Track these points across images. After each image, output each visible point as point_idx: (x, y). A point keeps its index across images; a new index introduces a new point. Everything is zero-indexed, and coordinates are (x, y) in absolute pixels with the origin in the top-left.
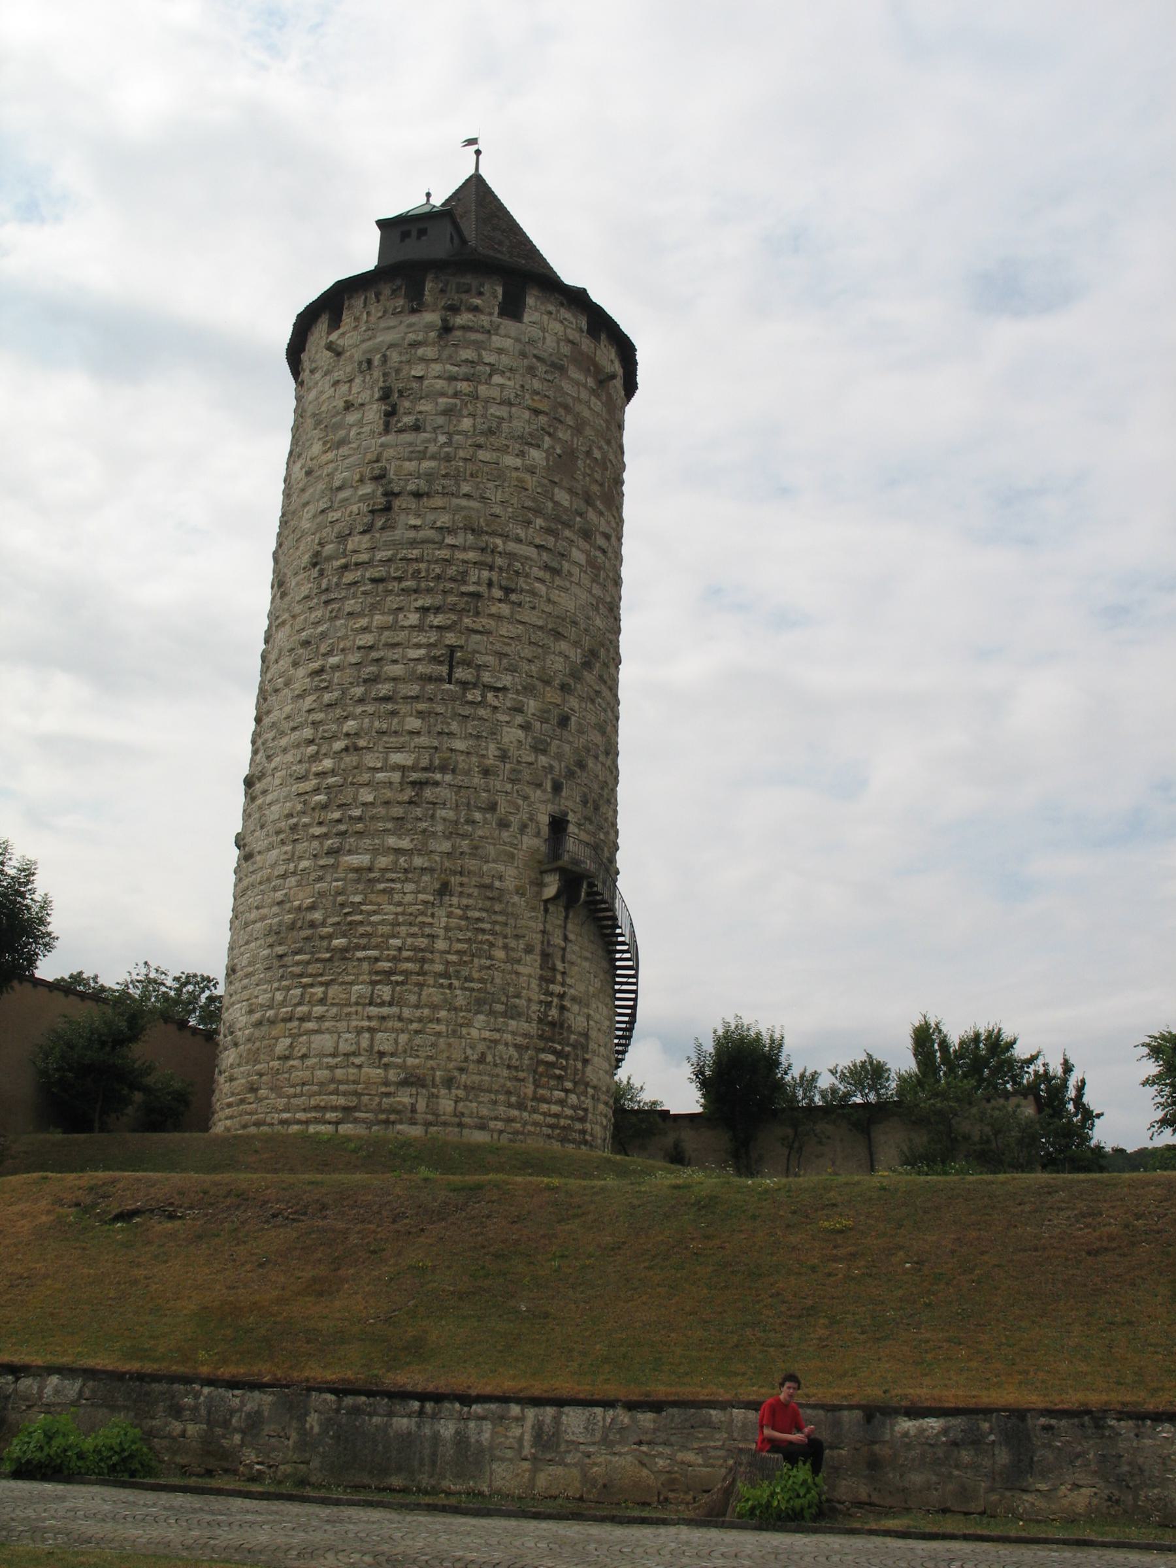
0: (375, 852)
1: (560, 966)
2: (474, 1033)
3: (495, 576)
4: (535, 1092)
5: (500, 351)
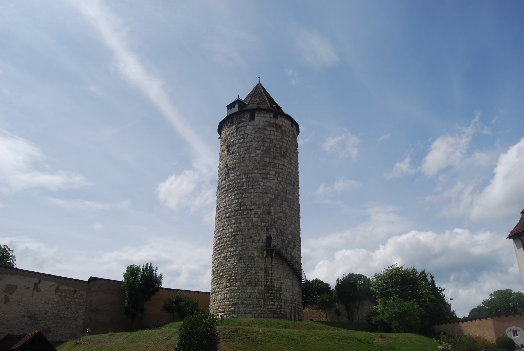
0: (227, 252)
1: (270, 272)
2: (248, 291)
3: (250, 183)
5: (249, 130)
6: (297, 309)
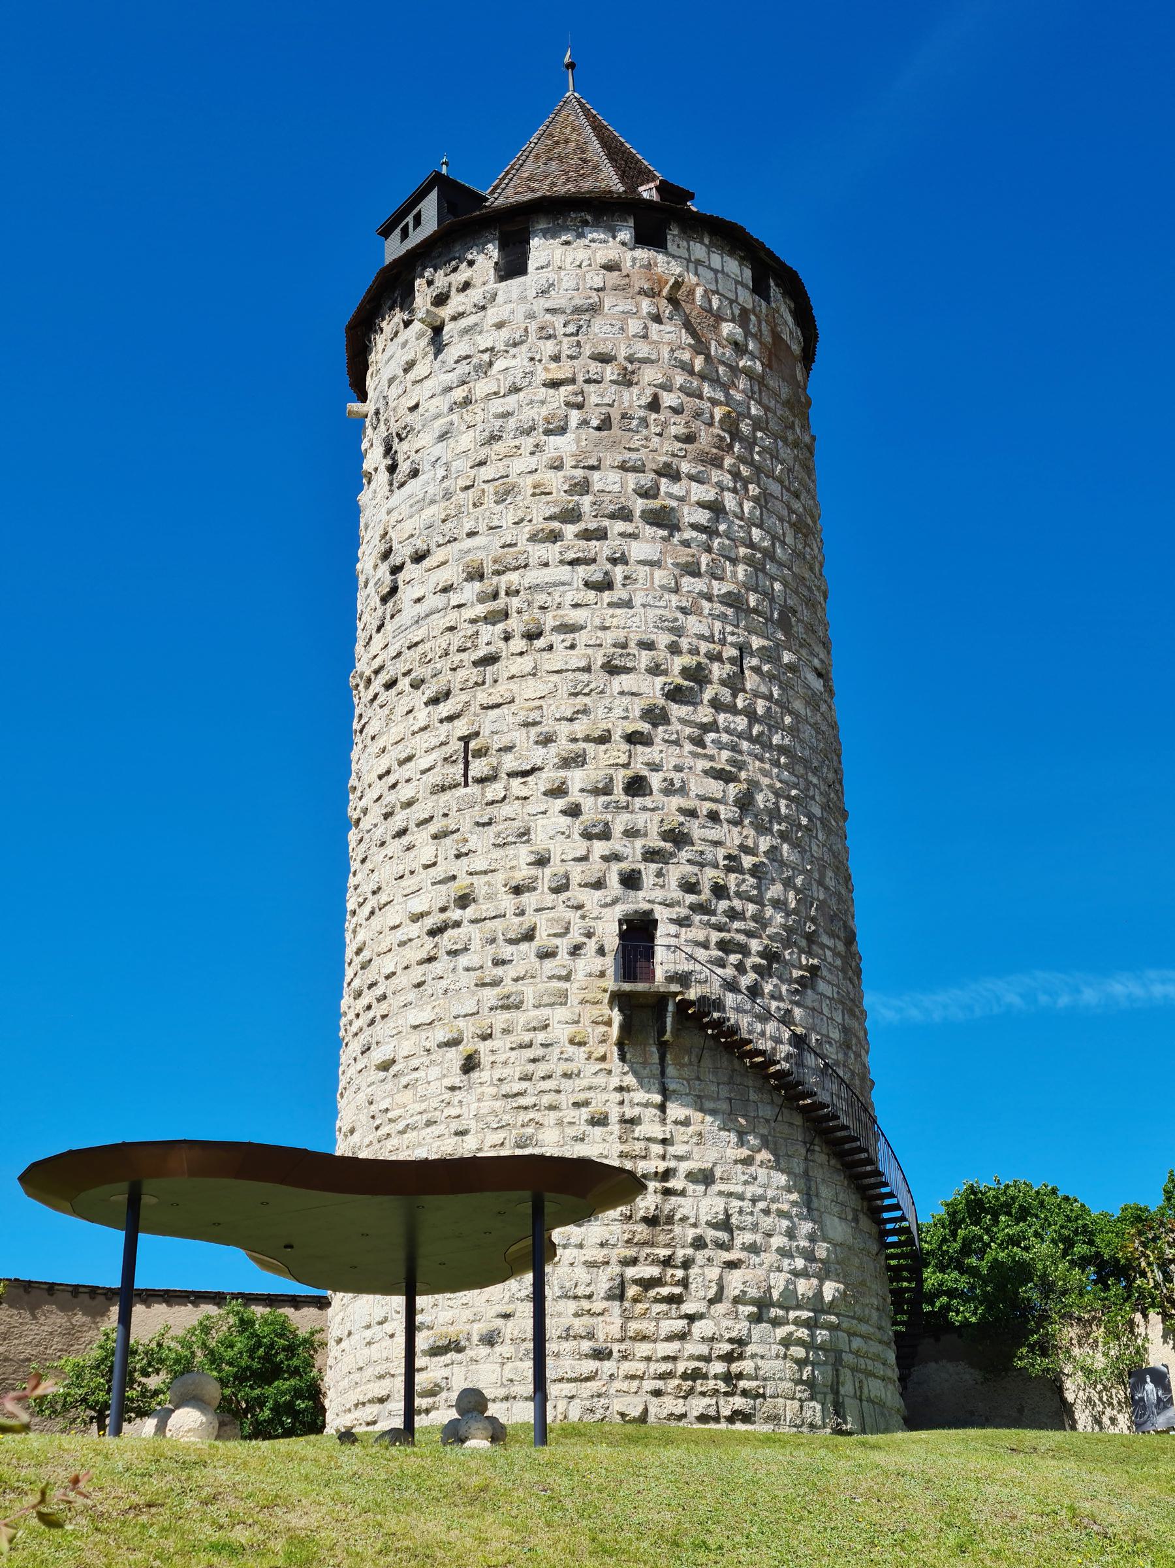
4: (623, 1328)
6: (848, 1358)
